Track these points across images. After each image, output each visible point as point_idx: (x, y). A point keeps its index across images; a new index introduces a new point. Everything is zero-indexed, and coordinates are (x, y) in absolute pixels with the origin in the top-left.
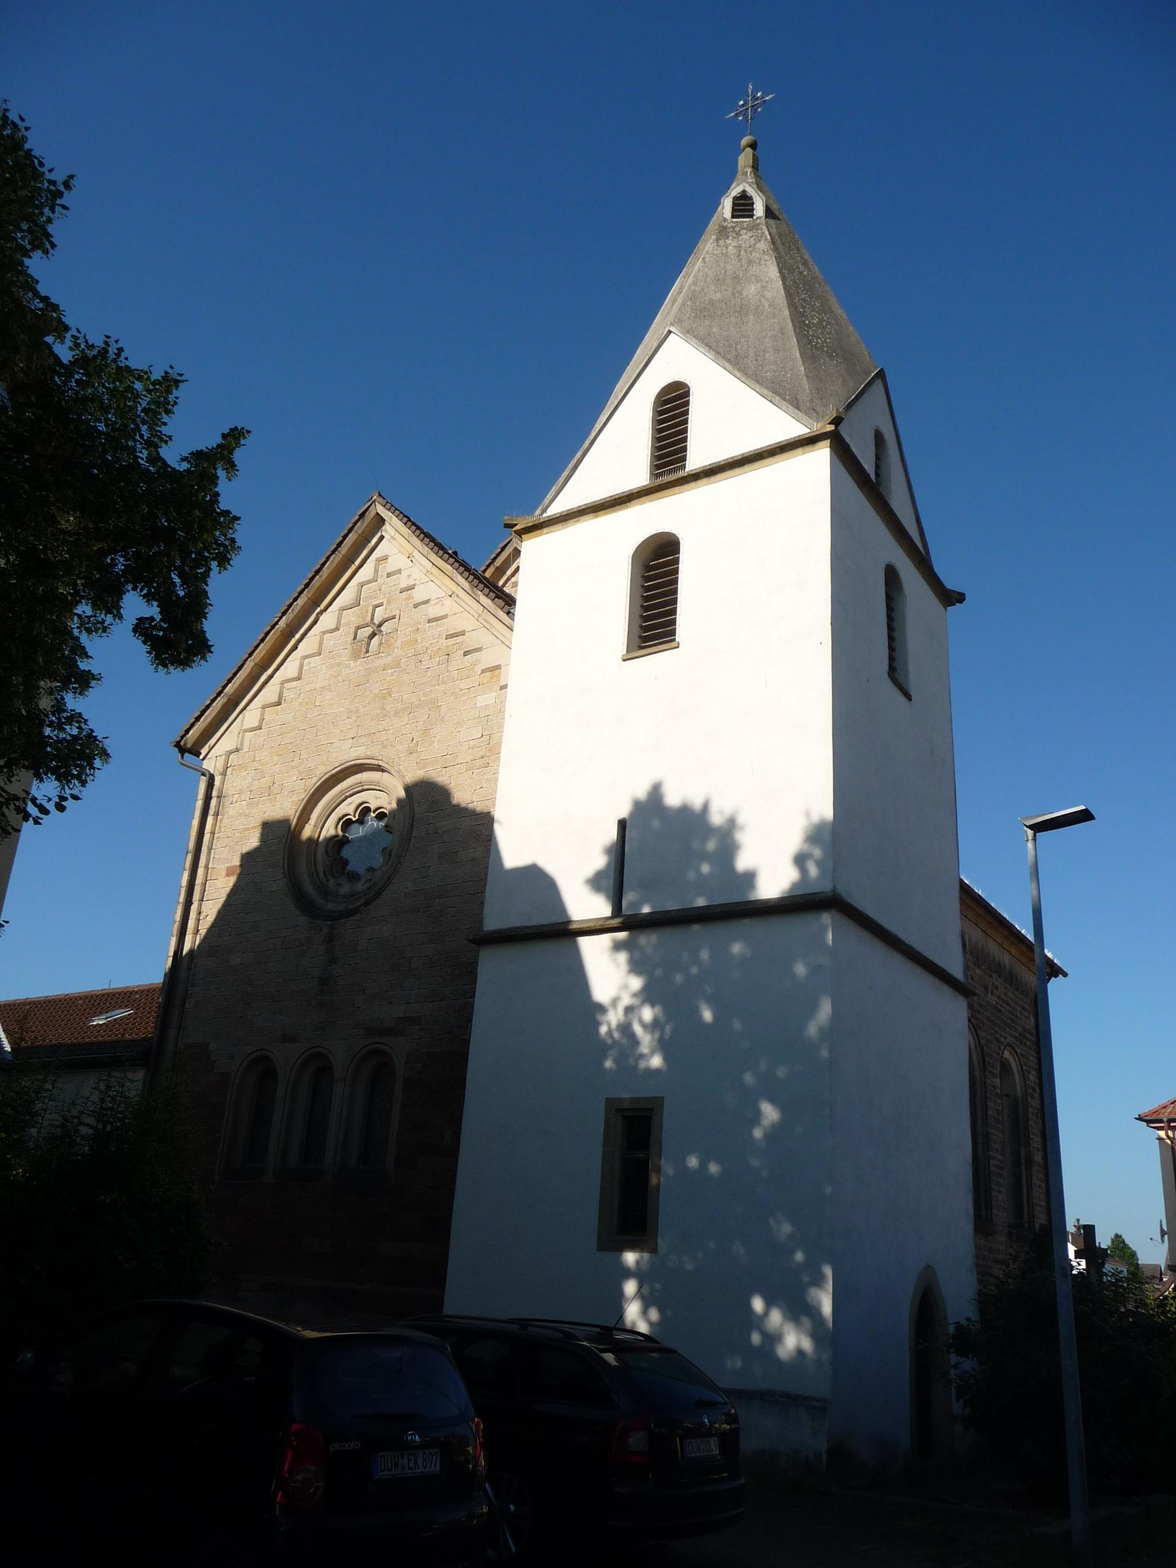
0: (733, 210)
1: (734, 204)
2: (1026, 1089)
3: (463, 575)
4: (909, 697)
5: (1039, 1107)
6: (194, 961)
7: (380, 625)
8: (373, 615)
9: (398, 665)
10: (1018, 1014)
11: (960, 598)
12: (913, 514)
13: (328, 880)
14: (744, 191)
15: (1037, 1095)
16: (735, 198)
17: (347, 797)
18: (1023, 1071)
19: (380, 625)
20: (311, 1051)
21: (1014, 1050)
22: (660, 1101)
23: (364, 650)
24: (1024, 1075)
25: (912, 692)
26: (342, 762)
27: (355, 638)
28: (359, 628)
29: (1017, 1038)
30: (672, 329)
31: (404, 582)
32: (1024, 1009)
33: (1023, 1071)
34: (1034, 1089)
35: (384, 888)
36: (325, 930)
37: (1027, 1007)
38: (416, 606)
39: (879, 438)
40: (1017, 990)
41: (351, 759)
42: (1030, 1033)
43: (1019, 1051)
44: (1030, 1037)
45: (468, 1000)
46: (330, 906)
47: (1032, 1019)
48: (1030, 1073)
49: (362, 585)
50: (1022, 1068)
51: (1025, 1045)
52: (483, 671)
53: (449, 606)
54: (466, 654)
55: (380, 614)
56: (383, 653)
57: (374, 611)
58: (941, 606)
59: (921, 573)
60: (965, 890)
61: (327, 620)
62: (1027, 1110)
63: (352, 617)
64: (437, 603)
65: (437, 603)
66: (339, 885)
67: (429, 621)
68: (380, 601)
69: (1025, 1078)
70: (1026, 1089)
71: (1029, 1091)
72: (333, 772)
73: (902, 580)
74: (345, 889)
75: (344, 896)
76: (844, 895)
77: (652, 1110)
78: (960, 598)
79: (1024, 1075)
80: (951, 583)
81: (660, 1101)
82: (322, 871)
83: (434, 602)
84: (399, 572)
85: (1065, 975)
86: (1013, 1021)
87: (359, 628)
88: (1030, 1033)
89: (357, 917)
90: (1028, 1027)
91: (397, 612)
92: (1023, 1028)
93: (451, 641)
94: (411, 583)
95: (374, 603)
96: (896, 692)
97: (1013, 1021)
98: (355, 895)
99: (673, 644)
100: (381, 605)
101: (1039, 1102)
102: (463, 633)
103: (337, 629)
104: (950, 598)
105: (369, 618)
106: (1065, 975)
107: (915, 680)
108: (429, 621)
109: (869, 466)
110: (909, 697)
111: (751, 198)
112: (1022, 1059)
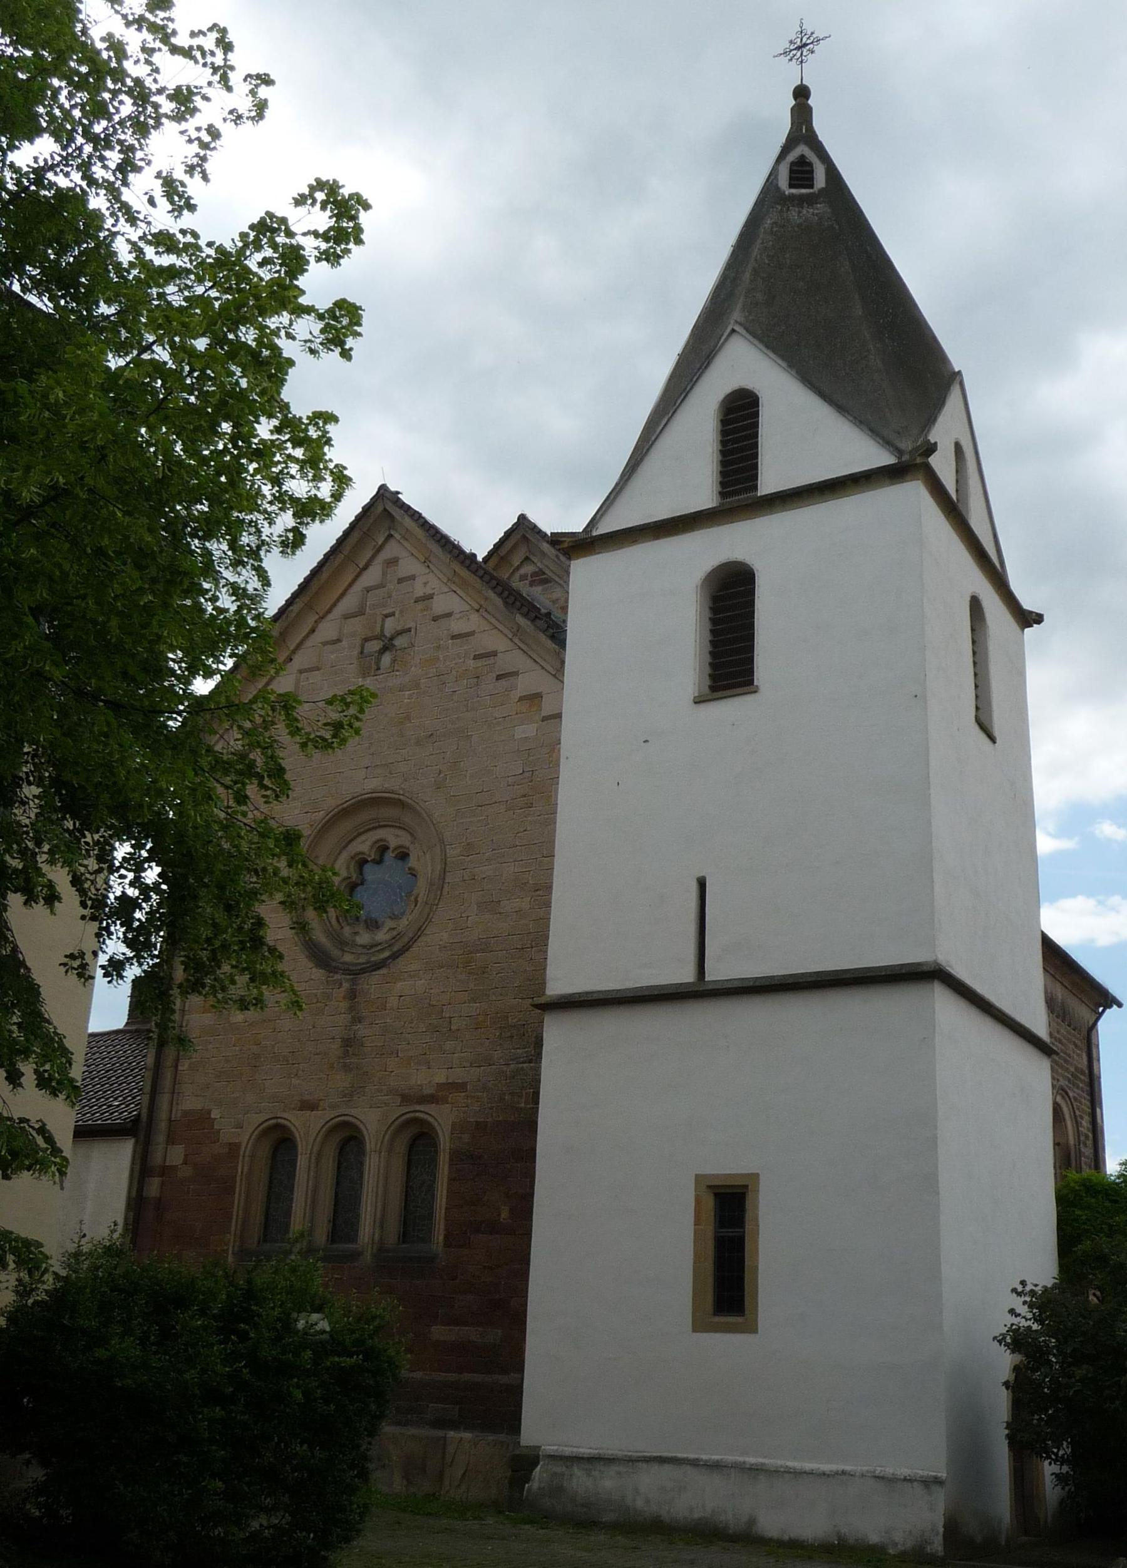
0: (791, 178)
1: (791, 171)
2: (1079, 1137)
3: (496, 590)
4: (993, 740)
5: (1091, 1156)
6: (186, 1017)
7: (392, 639)
8: (382, 626)
9: (417, 686)
10: (1071, 1053)
11: (1038, 619)
12: (990, 529)
13: (342, 928)
14: (802, 156)
15: (1090, 1143)
16: (792, 164)
17: (360, 834)
18: (1075, 1116)
19: (392, 639)
20: (337, 1119)
21: (1067, 1093)
22: (756, 1176)
23: (374, 666)
24: (1077, 1122)
25: (997, 733)
26: (355, 795)
27: (362, 653)
28: (366, 640)
29: (1069, 1081)
30: (737, 328)
31: (419, 591)
32: (1076, 1046)
33: (1075, 1116)
34: (1087, 1137)
35: (414, 940)
36: (346, 985)
37: (1079, 1043)
38: (435, 619)
39: (958, 448)
40: (1069, 1026)
41: (366, 791)
42: (1083, 1073)
43: (1071, 1094)
44: (1082, 1077)
45: (521, 1065)
46: (348, 958)
47: (1084, 1056)
48: (1082, 1118)
49: (368, 590)
50: (1075, 1113)
51: (1078, 1087)
52: (521, 699)
53: (474, 622)
54: (499, 677)
55: (390, 626)
56: (397, 671)
57: (383, 621)
58: (1018, 628)
59: (941, 510)
60: (1047, 943)
61: (327, 630)
62: (1080, 1160)
63: (357, 626)
64: (460, 618)
65: (460, 618)
66: (356, 933)
67: (454, 637)
68: (391, 610)
69: (1077, 1124)
70: (1079, 1137)
71: (1082, 1138)
72: (345, 805)
73: (985, 610)
74: (364, 938)
75: (364, 947)
76: (944, 964)
77: (746, 1187)
78: (1038, 619)
79: (1077, 1122)
80: (1027, 604)
81: (756, 1176)
82: (334, 917)
83: (458, 616)
84: (413, 578)
85: (1120, 1005)
86: (1066, 1061)
87: (366, 640)
88: (1083, 1073)
89: (383, 971)
90: (1079, 1066)
91: (412, 625)
92: (1076, 1069)
93: (479, 663)
94: (429, 591)
95: (384, 612)
96: (983, 737)
97: (1066, 1061)
98: (376, 945)
99: (751, 688)
100: (393, 614)
101: (1092, 1151)
102: (494, 654)
103: (339, 640)
104: (1027, 619)
105: (378, 629)
106: (1120, 1005)
107: (999, 723)
108: (454, 637)
109: (951, 487)
110: (993, 740)
111: (810, 164)
112: (1075, 1104)
